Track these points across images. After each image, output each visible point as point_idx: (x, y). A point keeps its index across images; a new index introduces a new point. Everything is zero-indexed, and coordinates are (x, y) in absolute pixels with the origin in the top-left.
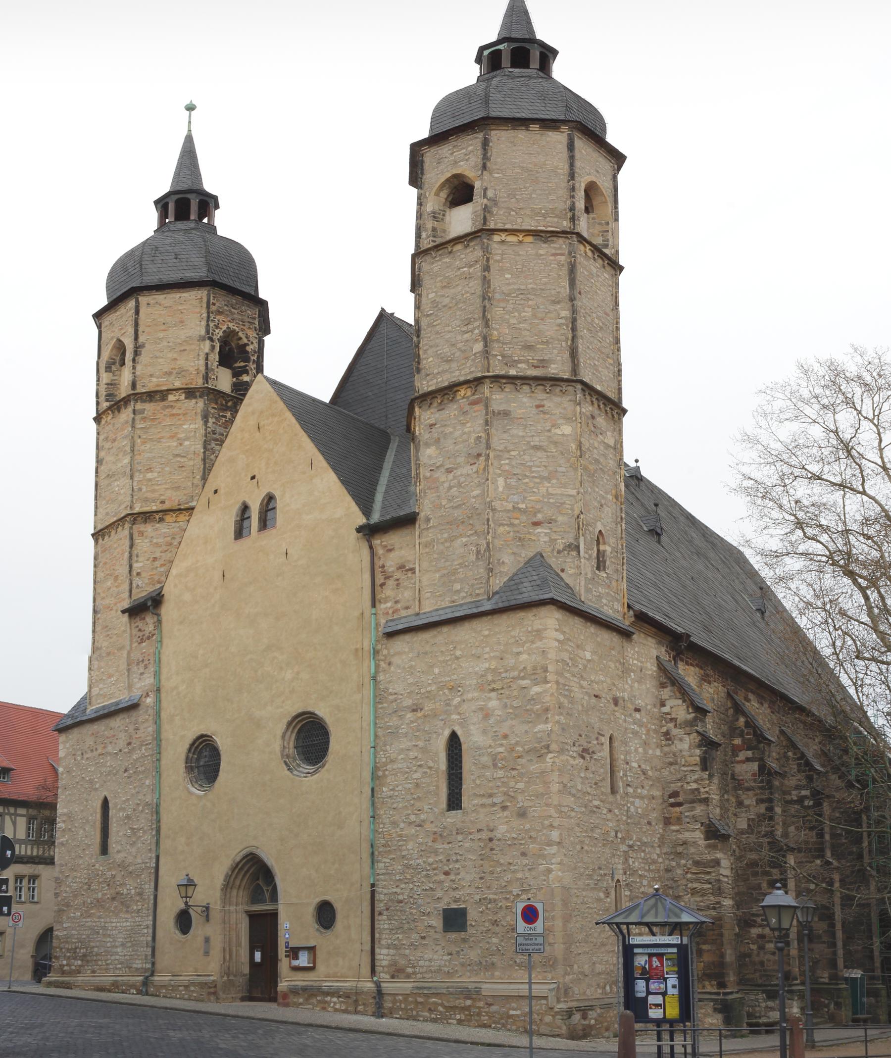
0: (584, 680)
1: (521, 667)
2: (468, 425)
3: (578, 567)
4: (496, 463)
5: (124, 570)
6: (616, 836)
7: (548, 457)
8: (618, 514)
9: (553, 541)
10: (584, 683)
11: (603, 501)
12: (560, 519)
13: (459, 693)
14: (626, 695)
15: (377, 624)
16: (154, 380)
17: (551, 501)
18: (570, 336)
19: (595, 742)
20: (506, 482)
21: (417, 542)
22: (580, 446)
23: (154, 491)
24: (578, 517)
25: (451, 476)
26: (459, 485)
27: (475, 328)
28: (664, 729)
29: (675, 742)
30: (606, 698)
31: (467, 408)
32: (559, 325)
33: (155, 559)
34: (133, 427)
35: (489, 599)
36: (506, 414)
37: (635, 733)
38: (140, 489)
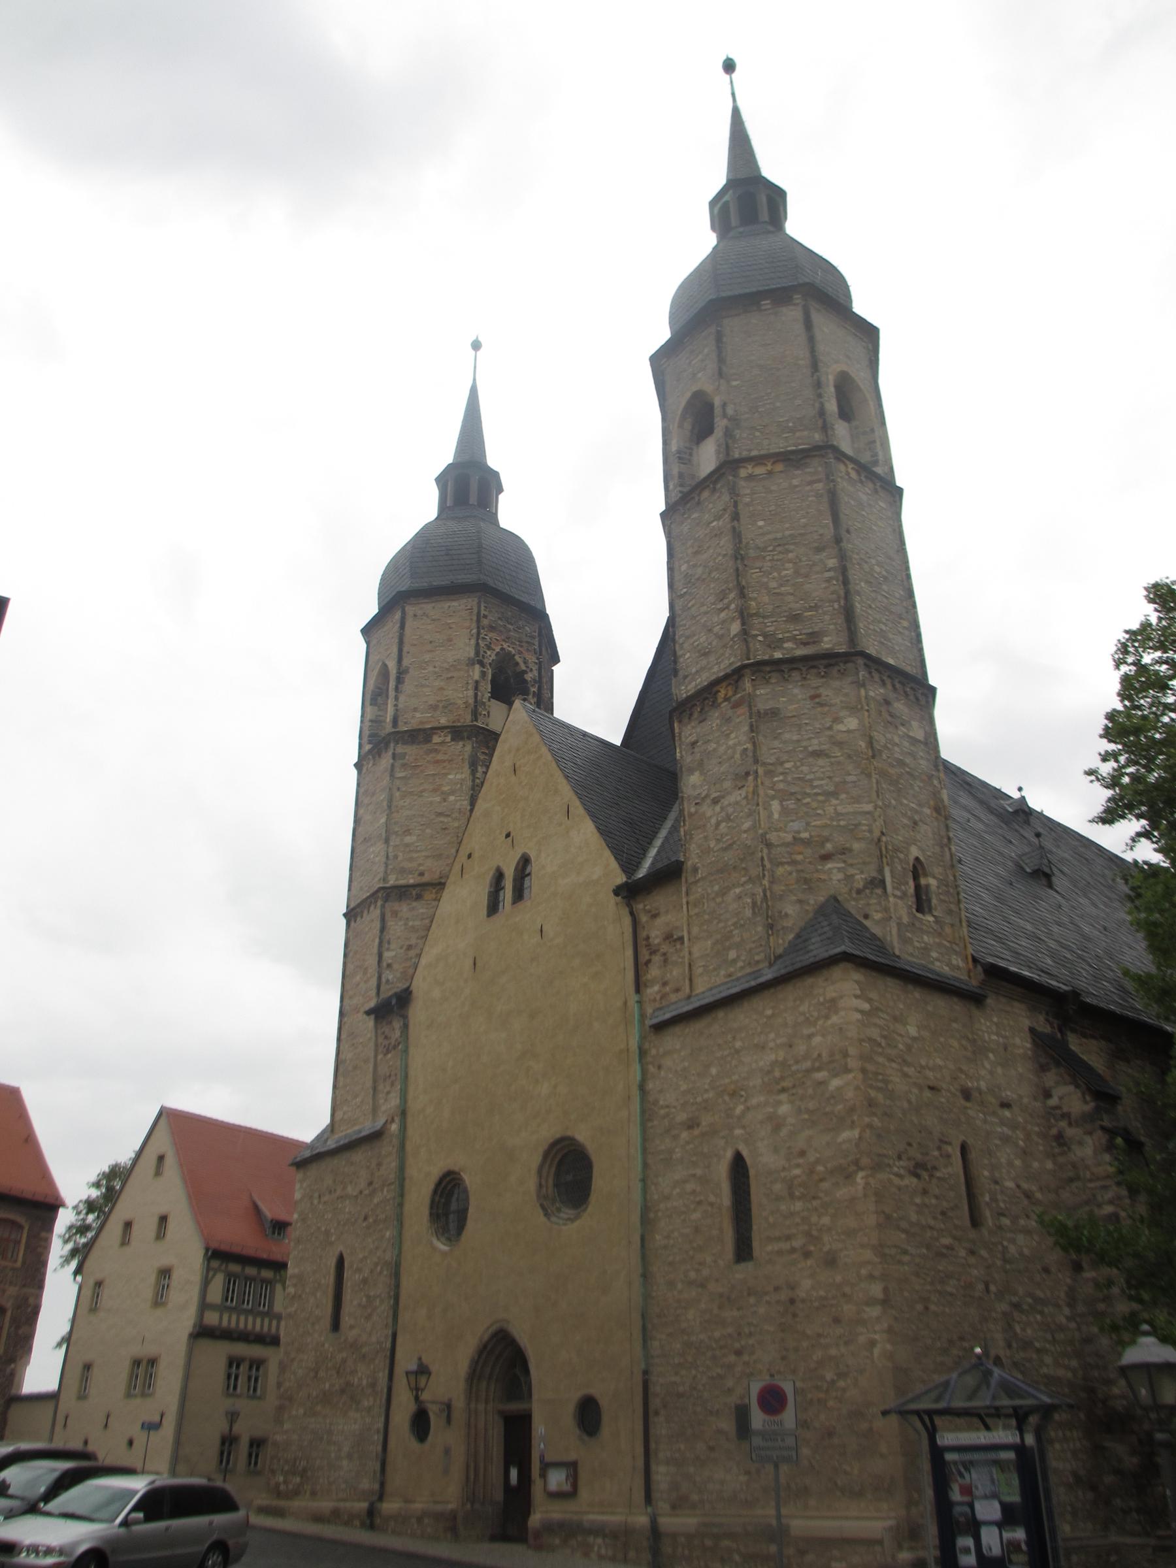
0: (909, 1065)
1: (815, 1055)
2: (733, 736)
3: (886, 910)
4: (767, 783)
5: (372, 961)
6: (987, 1290)
7: (832, 764)
8: (943, 833)
9: (849, 878)
10: (911, 1071)
11: (917, 817)
12: (856, 846)
13: (743, 1099)
14: (983, 1085)
15: (643, 1016)
16: (418, 715)
17: (842, 823)
18: (842, 593)
19: (936, 1153)
20: (782, 805)
21: (684, 901)
22: (870, 744)
23: (411, 860)
24: (879, 840)
25: (718, 808)
26: (728, 818)
27: (730, 603)
28: (1054, 1131)
29: (1073, 1147)
30: (949, 1091)
31: (730, 713)
32: (828, 580)
33: (410, 947)
34: (392, 775)
35: (771, 965)
36: (774, 713)
37: (1006, 1139)
38: (396, 857)
